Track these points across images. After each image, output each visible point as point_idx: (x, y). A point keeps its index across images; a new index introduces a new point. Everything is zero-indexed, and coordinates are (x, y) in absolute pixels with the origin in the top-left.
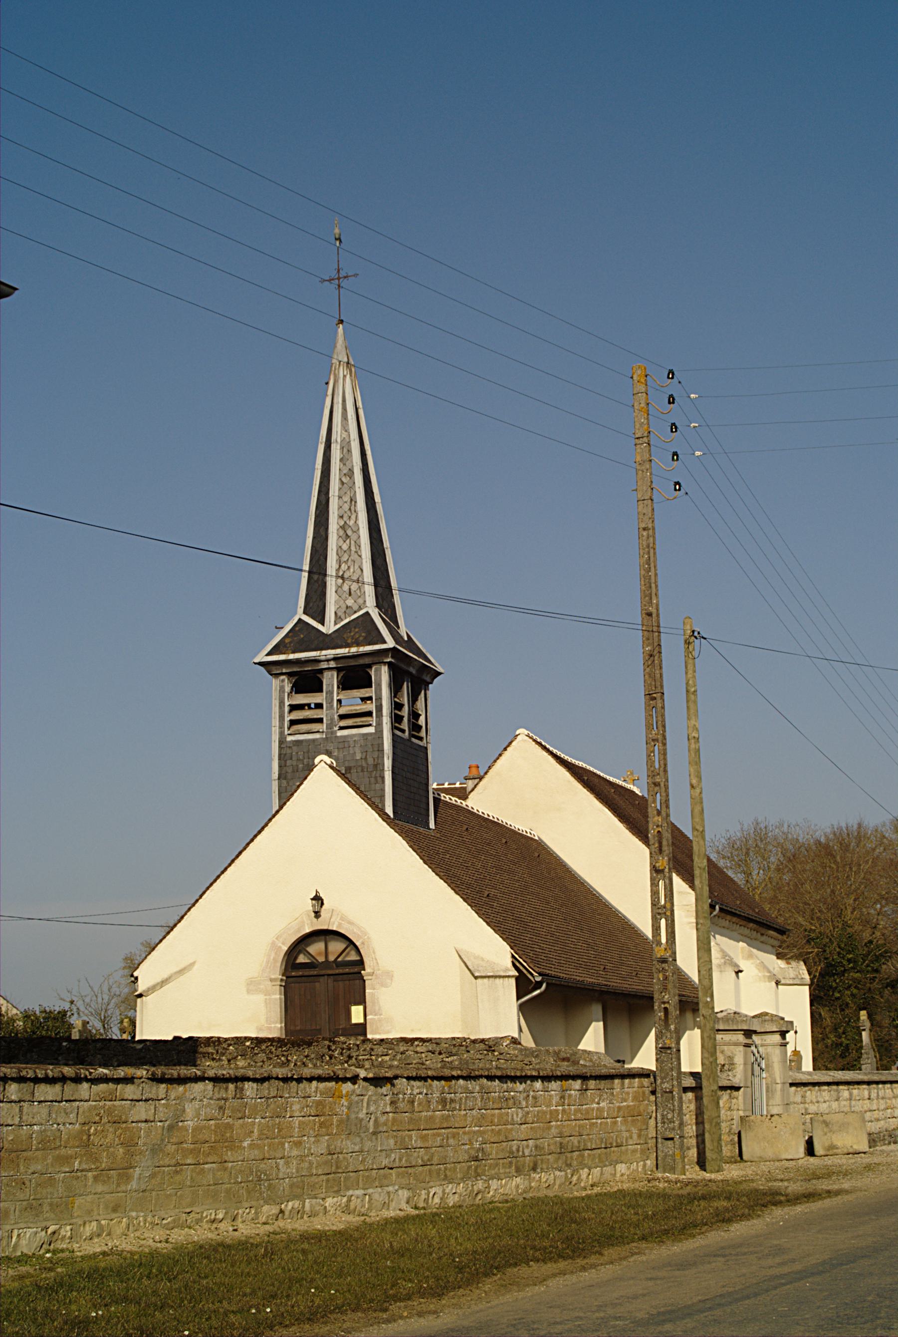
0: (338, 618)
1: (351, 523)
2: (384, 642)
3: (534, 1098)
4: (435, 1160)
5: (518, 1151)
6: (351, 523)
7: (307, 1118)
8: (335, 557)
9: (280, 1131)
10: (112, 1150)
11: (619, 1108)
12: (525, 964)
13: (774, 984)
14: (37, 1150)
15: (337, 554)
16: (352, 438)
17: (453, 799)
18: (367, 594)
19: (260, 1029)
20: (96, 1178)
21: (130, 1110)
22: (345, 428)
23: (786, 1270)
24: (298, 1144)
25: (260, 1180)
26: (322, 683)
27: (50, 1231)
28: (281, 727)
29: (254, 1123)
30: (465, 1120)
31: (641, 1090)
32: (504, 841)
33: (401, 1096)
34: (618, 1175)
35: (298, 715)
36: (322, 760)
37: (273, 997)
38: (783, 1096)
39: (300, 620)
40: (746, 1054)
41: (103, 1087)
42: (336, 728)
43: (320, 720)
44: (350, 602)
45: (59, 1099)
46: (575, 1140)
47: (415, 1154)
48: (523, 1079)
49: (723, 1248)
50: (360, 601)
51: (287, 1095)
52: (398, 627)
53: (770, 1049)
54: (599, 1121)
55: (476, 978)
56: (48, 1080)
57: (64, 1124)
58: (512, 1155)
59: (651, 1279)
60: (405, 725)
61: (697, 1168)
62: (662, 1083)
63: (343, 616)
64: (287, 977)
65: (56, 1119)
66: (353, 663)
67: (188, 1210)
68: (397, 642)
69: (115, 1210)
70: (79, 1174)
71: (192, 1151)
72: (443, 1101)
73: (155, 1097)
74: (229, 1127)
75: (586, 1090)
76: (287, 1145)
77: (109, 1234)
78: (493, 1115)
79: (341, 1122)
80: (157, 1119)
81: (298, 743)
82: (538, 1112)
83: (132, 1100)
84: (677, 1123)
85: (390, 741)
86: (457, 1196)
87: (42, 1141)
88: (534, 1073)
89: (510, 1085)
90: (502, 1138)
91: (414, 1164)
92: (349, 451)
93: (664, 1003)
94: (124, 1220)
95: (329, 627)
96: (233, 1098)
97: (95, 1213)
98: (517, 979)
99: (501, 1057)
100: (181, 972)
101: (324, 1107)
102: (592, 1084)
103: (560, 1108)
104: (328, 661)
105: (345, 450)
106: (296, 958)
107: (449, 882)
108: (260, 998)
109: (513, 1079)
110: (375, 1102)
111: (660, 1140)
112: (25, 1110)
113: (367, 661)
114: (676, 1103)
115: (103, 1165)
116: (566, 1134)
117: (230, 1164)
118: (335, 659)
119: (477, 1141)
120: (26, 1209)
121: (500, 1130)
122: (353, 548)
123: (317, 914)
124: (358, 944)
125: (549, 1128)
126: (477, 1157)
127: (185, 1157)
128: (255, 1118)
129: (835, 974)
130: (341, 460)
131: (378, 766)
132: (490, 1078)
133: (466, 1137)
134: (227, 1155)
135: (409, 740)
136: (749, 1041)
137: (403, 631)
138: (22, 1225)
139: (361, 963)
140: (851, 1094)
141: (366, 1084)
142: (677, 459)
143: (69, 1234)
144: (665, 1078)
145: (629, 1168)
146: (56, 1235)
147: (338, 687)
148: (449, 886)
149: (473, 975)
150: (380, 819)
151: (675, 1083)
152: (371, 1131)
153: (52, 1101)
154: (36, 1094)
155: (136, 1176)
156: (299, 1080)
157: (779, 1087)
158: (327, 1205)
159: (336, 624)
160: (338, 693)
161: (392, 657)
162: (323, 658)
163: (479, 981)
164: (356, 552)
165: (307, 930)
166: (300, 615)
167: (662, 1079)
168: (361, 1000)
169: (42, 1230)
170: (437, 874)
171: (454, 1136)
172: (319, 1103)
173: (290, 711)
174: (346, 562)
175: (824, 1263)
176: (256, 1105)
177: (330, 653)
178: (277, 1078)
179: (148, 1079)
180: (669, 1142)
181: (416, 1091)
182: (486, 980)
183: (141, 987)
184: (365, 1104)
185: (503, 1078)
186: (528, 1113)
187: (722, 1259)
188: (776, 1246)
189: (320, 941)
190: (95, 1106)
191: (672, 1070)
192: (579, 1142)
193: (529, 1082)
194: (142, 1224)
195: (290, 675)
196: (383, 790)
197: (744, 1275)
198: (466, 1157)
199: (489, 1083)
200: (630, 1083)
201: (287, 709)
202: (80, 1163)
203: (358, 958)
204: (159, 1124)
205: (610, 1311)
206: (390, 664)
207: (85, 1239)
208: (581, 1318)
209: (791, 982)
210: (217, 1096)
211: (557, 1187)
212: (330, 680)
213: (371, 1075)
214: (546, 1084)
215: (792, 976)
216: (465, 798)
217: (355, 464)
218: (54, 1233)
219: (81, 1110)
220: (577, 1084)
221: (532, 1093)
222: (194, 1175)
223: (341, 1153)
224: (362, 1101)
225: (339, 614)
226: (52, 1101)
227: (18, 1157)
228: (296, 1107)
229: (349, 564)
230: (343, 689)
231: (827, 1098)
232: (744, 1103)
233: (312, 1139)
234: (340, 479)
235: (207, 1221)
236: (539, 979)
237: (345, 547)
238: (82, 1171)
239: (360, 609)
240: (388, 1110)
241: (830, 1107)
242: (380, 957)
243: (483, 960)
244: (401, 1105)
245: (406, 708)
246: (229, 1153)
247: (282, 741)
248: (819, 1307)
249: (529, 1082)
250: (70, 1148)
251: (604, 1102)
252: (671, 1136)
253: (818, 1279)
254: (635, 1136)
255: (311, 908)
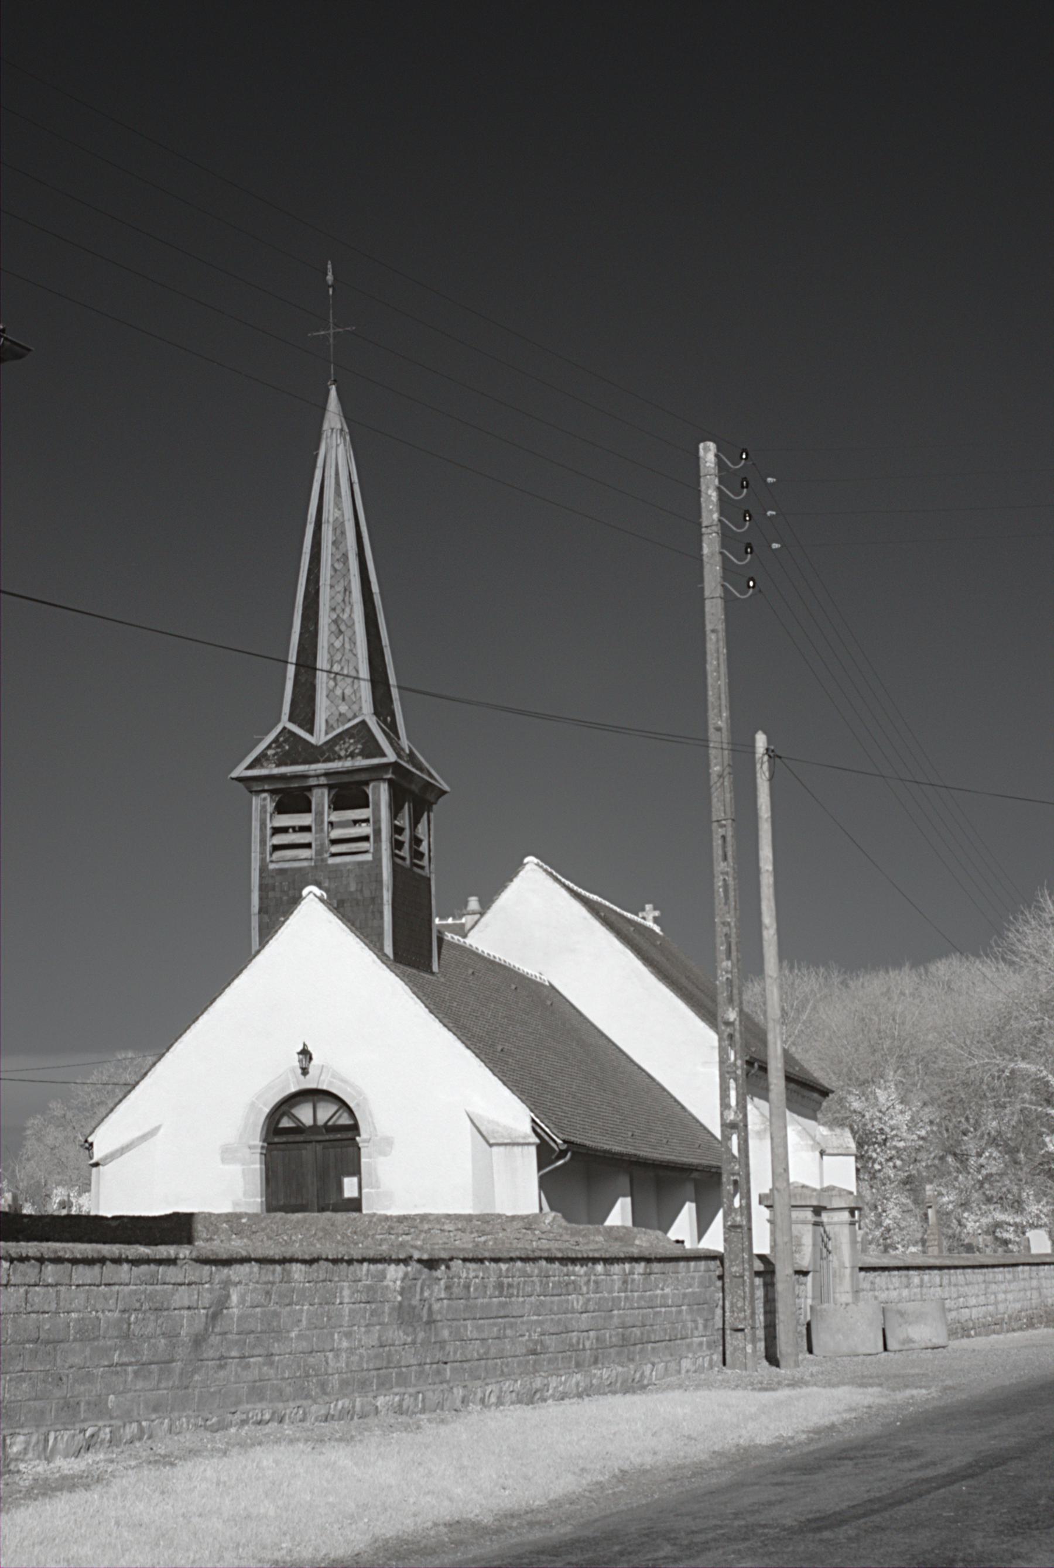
0: (329, 727)
1: (345, 616)
2: (384, 755)
3: (596, 1282)
4: (493, 1351)
5: (578, 1343)
6: (345, 616)
7: (357, 1306)
8: (326, 656)
9: (329, 1319)
10: (153, 1341)
11: (685, 1295)
12: (547, 1130)
13: (818, 1154)
14: (75, 1340)
15: (329, 652)
16: (346, 517)
17: (456, 937)
18: (363, 699)
19: (236, 1204)
20: (136, 1373)
21: (173, 1295)
22: (338, 505)
23: (930, 1473)
24: (348, 1335)
25: (308, 1376)
26: (309, 802)
27: (88, 1434)
28: (263, 852)
29: (302, 1311)
30: (524, 1308)
31: (707, 1275)
32: (513, 987)
33: (456, 1280)
34: (683, 1371)
35: (279, 839)
36: (311, 892)
37: (252, 1166)
38: (852, 1280)
39: (284, 728)
40: (814, 1233)
41: (144, 1268)
42: (326, 855)
43: (308, 846)
44: (343, 708)
45: (97, 1283)
46: (637, 1331)
47: (471, 1347)
48: (584, 1261)
49: (844, 1450)
50: (355, 707)
51: (336, 1279)
52: (399, 738)
53: (837, 1228)
54: (663, 1310)
55: (491, 1145)
56: (89, 1262)
57: (103, 1312)
58: (574, 1348)
59: (777, 1484)
60: (405, 852)
61: (765, 1363)
62: (731, 1266)
63: (335, 725)
64: (269, 1144)
65: (94, 1306)
66: (346, 779)
67: (233, 1410)
68: (399, 755)
69: (155, 1410)
70: (119, 1369)
71: (237, 1342)
72: (500, 1286)
73: (198, 1280)
74: (276, 1315)
75: (650, 1274)
76: (336, 1336)
77: (150, 1438)
78: (552, 1302)
79: (392, 1309)
80: (200, 1306)
81: (282, 871)
82: (600, 1298)
83: (174, 1284)
84: (748, 1312)
85: (390, 870)
86: (514, 1395)
87: (80, 1330)
88: (597, 1255)
89: (570, 1268)
90: (561, 1328)
91: (469, 1357)
92: (343, 533)
93: (733, 1174)
94: (166, 1421)
95: (319, 737)
96: (281, 1282)
97: (135, 1413)
98: (539, 1148)
99: (544, 1236)
100: (144, 1138)
101: (375, 1292)
102: (656, 1267)
103: (623, 1294)
104: (318, 776)
105: (338, 532)
106: (278, 1122)
107: (459, 1034)
108: (236, 1169)
109: (574, 1261)
110: (429, 1287)
111: (728, 1332)
112: (62, 1296)
113: (363, 777)
114: (747, 1289)
115: (144, 1358)
116: (628, 1324)
117: (277, 1358)
118: (326, 775)
119: (535, 1332)
120: (62, 1409)
121: (560, 1319)
122: (347, 646)
123: (305, 1071)
124: (352, 1105)
125: (611, 1317)
126: (535, 1350)
127: (229, 1349)
128: (303, 1305)
129: (875, 1143)
130: (334, 543)
131: (376, 900)
132: (550, 1260)
133: (524, 1327)
134: (273, 1347)
135: (411, 870)
136: (817, 1219)
137: (405, 743)
138: (58, 1427)
139: (355, 1128)
140: (922, 1280)
141: (419, 1266)
142: (751, 552)
143: (108, 1437)
144: (735, 1260)
145: (694, 1363)
146: (95, 1438)
147: (329, 807)
148: (459, 1038)
149: (487, 1142)
150: (378, 961)
151: (746, 1266)
152: (425, 1319)
153: (90, 1285)
154: (74, 1276)
155: (178, 1371)
156: (350, 1262)
157: (848, 1271)
158: (378, 1404)
159: (327, 733)
160: (329, 815)
161: (393, 773)
162: (312, 773)
163: (495, 1149)
164: (351, 650)
165: (293, 1089)
166: (285, 722)
167: (731, 1261)
168: (356, 1171)
169: (80, 1432)
170: (445, 1026)
171: (512, 1326)
172: (369, 1288)
173: (273, 834)
174: (339, 662)
175: (970, 1466)
176: (304, 1289)
177: (321, 767)
178: (327, 1260)
179: (192, 1259)
180: (739, 1334)
181: (472, 1275)
182: (502, 1148)
183: (98, 1154)
184: (418, 1289)
185: (565, 1260)
186: (589, 1300)
187: (850, 1463)
188: (906, 1447)
189: (306, 1101)
190: (136, 1291)
191: (743, 1250)
192: (642, 1334)
193: (590, 1265)
194: (185, 1426)
195: (272, 792)
196: (381, 927)
197: (884, 1479)
198: (524, 1351)
199: (549, 1266)
200: (696, 1267)
201: (269, 832)
202: (120, 1355)
203: (351, 1122)
204: (202, 1311)
205: (751, 1519)
206: (390, 781)
207: (126, 1443)
208: (721, 1527)
209: (835, 1152)
210: (264, 1279)
211: (619, 1384)
212: (321, 798)
213: (425, 1257)
214: (608, 1266)
215: (835, 1144)
216: (465, 936)
217: (349, 548)
218: (92, 1436)
219: (121, 1295)
220: (640, 1267)
221: (593, 1278)
222: (239, 1369)
223: (393, 1345)
224: (415, 1285)
225: (331, 722)
226: (90, 1285)
227: (55, 1349)
228: (346, 1293)
229: (343, 663)
230: (335, 809)
231: (897, 1285)
232: (813, 1291)
233: (363, 1329)
234: (332, 565)
235: (253, 1423)
236: (564, 1147)
237: (338, 644)
238: (122, 1365)
239: (355, 716)
240: (443, 1295)
241: (900, 1294)
242: (380, 1119)
243: (498, 1124)
244: (456, 1290)
245: (407, 832)
246: (276, 1345)
247: (263, 869)
248: (988, 1512)
249: (590, 1265)
250: (110, 1338)
251: (671, 1286)
252: (741, 1327)
253: (972, 1482)
254: (701, 1327)
255: (297, 1064)
